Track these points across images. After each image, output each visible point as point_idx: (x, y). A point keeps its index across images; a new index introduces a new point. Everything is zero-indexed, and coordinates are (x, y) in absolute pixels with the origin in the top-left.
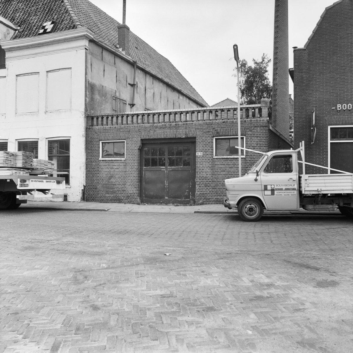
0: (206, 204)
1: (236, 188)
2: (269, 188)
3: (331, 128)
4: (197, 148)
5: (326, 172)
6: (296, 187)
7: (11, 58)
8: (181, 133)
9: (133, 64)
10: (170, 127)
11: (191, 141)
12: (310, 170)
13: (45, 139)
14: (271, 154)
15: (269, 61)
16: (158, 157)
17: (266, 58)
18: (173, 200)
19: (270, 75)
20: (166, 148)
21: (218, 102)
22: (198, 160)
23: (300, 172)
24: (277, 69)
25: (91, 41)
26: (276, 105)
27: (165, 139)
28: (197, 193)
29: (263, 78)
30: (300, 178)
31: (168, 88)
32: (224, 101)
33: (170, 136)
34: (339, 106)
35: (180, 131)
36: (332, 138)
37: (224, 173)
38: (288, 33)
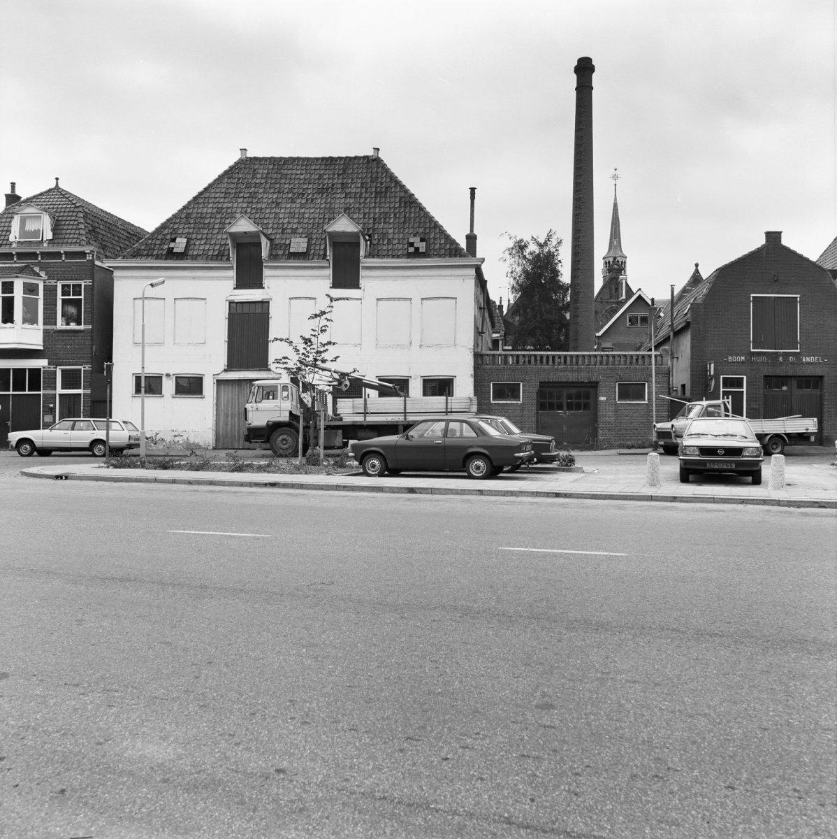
0: (609, 449)
4: (600, 392)
7: (408, 277)
8: (584, 377)
11: (594, 385)
13: (419, 378)
18: (572, 446)
20: (565, 392)
24: (579, 261)
26: (578, 316)
28: (600, 437)
34: (730, 358)
37: (627, 418)
38: (593, 210)
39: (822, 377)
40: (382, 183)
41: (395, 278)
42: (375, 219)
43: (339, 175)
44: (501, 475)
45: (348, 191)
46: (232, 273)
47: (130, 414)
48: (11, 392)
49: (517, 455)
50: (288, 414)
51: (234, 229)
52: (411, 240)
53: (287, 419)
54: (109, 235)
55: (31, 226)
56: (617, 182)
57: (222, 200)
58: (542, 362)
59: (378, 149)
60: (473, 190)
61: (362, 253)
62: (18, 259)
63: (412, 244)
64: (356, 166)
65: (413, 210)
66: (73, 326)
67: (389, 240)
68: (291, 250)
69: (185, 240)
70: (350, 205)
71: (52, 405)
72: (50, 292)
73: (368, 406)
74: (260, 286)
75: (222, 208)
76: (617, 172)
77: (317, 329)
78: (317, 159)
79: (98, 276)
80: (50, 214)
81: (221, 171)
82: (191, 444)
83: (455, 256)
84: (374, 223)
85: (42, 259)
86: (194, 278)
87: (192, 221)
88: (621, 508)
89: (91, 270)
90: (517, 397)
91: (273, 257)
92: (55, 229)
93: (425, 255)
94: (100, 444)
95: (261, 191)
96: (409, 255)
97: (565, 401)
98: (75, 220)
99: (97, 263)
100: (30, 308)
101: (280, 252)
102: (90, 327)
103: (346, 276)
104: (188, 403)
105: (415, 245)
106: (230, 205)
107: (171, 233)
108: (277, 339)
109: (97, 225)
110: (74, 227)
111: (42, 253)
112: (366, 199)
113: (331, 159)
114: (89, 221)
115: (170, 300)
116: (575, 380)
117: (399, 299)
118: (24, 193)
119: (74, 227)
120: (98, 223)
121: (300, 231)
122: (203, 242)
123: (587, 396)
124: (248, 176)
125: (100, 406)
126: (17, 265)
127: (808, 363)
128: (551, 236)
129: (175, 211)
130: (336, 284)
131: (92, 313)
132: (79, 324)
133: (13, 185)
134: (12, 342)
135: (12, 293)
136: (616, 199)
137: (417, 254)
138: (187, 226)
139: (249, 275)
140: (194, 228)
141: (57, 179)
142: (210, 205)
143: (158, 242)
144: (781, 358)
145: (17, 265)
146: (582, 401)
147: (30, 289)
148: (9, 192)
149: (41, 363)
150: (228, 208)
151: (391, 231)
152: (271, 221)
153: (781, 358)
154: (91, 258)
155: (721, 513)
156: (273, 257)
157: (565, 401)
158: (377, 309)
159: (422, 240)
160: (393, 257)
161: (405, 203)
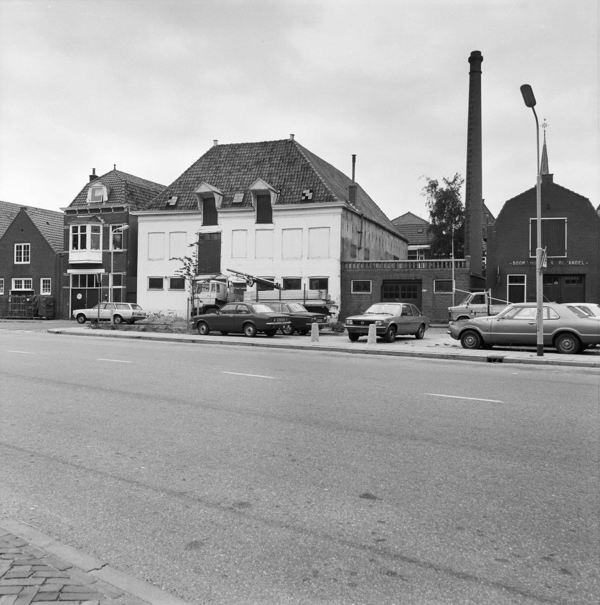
1: (457, 312)
2: (473, 311)
3: (509, 276)
5: (506, 303)
6: (487, 311)
9: (360, 216)
10: (404, 272)
11: (420, 282)
12: (494, 303)
14: (474, 294)
15: (462, 182)
16: (394, 292)
17: (459, 178)
19: (462, 198)
20: (400, 286)
21: (398, 217)
22: (423, 295)
23: (489, 304)
25: (344, 208)
27: (393, 280)
29: (456, 201)
30: (489, 307)
31: (377, 228)
32: (404, 215)
33: (404, 278)
34: (514, 262)
35: (411, 275)
36: (510, 282)
39: (584, 275)
40: (292, 156)
41: (293, 216)
42: (285, 179)
43: (268, 153)
44: (275, 336)
45: (272, 162)
46: (201, 217)
47: (149, 302)
48: (87, 288)
49: (268, 323)
50: (214, 300)
51: (199, 191)
52: (304, 192)
53: (214, 303)
54: (143, 196)
55: (98, 194)
56: (546, 129)
57: (200, 173)
58: (444, 266)
59: (293, 135)
60: (354, 156)
61: (273, 201)
62: (79, 213)
63: (304, 195)
64: (279, 146)
65: (308, 172)
66: (118, 250)
67: (291, 192)
68: (234, 201)
69: (177, 198)
70: (272, 171)
71: (106, 295)
72: (106, 231)
73: (259, 296)
74: (216, 223)
75: (199, 177)
76: (546, 122)
77: (195, 252)
78: (257, 143)
79: (131, 220)
80: (107, 186)
81: (201, 155)
82: (178, 318)
83: (330, 201)
84: (284, 182)
85: (102, 212)
86: (155, 221)
87: (182, 186)
88: (228, 349)
89: (127, 218)
90: (368, 290)
91: (223, 206)
92: (109, 196)
93: (312, 201)
94: (81, 316)
95: (223, 165)
96: (302, 202)
97: (400, 292)
98: (120, 189)
99: (130, 213)
100: (95, 240)
101: (228, 203)
102: (126, 250)
103: (265, 217)
104: (177, 293)
105: (306, 195)
106: (204, 175)
107: (170, 194)
108: (173, 258)
109: (134, 190)
110: (120, 193)
111: (102, 209)
112: (282, 167)
113: (266, 143)
114: (128, 189)
115: (167, 234)
116: (406, 278)
117: (296, 229)
118: (99, 174)
119: (120, 193)
120: (135, 189)
121: (241, 189)
122: (186, 198)
123: (415, 289)
124: (219, 159)
125: (131, 296)
126: (90, 216)
127: (573, 265)
128: (457, 177)
129: (174, 180)
130: (259, 221)
131: (127, 242)
132: (121, 249)
133: (94, 169)
134: (85, 259)
135: (85, 232)
136: (545, 142)
137: (307, 201)
138: (179, 189)
139: (210, 218)
140: (183, 190)
141: (115, 165)
142: (193, 176)
143: (163, 200)
144: (552, 262)
145: (90, 216)
146: (412, 292)
147: (95, 229)
148: (92, 174)
149: (102, 271)
150: (202, 177)
151: (293, 187)
152: (225, 184)
153: (552, 262)
154: (127, 211)
155: (341, 358)
156: (223, 206)
157: (400, 292)
158: (282, 235)
159: (311, 191)
160: (292, 203)
161: (305, 168)
